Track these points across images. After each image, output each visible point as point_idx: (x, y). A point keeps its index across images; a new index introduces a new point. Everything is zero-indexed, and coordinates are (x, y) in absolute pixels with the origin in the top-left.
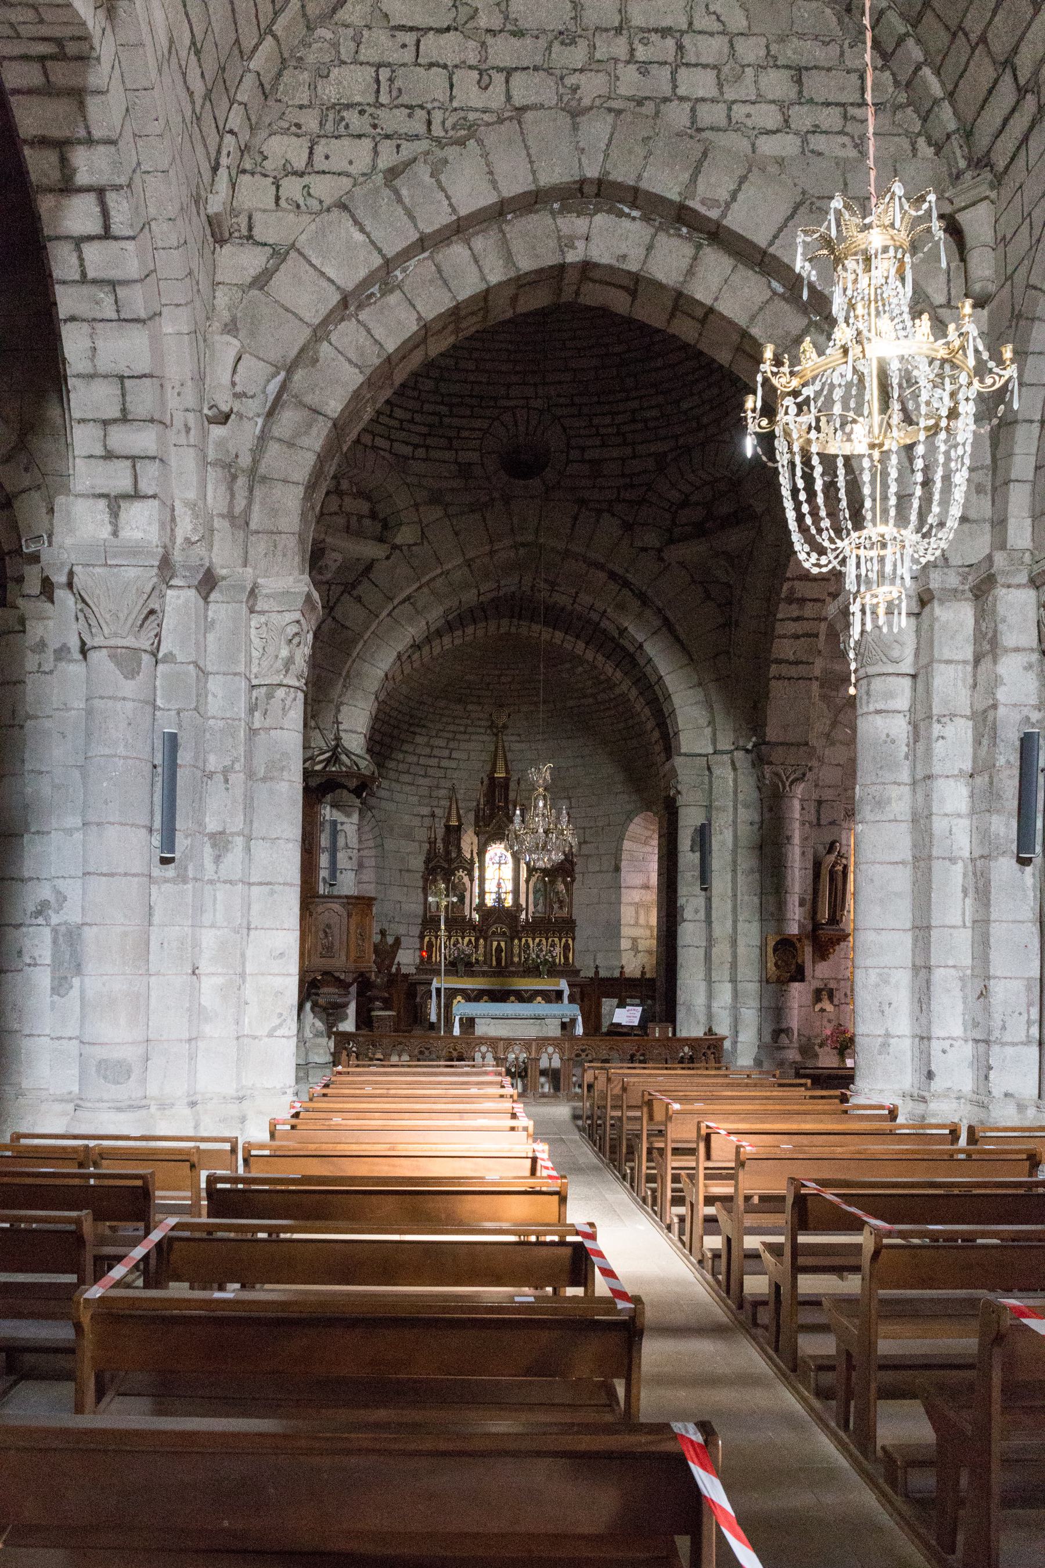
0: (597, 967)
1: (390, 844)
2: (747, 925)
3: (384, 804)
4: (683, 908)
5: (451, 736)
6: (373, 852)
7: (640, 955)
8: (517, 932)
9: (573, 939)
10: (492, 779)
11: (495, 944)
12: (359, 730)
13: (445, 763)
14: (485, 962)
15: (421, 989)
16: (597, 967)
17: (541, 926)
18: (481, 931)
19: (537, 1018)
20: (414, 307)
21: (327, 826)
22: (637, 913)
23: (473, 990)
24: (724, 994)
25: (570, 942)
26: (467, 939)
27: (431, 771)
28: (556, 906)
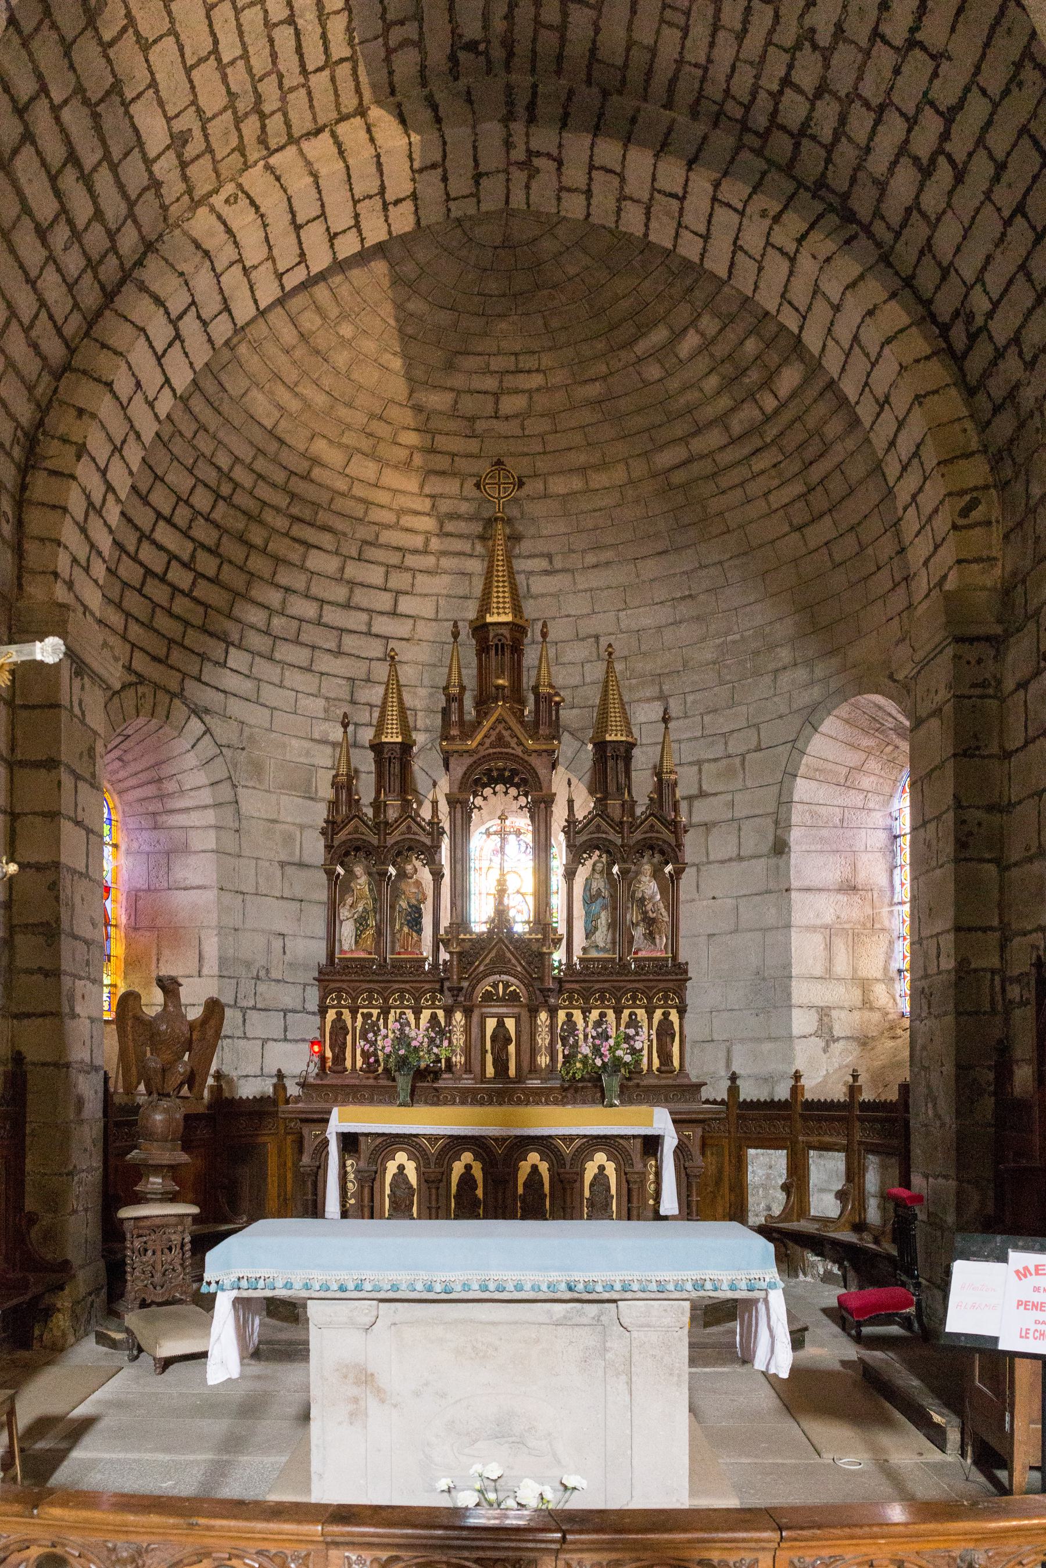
0: (734, 1078)
1: (253, 803)
3: (235, 707)
5: (394, 559)
6: (210, 817)
7: (837, 1047)
8: (545, 992)
9: (682, 1012)
10: (480, 629)
11: (491, 1024)
14: (468, 1068)
15: (310, 1132)
16: (734, 1078)
17: (605, 982)
18: (456, 991)
19: (581, 1297)
22: (829, 947)
23: (433, 1139)
25: (674, 1016)
27: (350, 642)
28: (639, 932)
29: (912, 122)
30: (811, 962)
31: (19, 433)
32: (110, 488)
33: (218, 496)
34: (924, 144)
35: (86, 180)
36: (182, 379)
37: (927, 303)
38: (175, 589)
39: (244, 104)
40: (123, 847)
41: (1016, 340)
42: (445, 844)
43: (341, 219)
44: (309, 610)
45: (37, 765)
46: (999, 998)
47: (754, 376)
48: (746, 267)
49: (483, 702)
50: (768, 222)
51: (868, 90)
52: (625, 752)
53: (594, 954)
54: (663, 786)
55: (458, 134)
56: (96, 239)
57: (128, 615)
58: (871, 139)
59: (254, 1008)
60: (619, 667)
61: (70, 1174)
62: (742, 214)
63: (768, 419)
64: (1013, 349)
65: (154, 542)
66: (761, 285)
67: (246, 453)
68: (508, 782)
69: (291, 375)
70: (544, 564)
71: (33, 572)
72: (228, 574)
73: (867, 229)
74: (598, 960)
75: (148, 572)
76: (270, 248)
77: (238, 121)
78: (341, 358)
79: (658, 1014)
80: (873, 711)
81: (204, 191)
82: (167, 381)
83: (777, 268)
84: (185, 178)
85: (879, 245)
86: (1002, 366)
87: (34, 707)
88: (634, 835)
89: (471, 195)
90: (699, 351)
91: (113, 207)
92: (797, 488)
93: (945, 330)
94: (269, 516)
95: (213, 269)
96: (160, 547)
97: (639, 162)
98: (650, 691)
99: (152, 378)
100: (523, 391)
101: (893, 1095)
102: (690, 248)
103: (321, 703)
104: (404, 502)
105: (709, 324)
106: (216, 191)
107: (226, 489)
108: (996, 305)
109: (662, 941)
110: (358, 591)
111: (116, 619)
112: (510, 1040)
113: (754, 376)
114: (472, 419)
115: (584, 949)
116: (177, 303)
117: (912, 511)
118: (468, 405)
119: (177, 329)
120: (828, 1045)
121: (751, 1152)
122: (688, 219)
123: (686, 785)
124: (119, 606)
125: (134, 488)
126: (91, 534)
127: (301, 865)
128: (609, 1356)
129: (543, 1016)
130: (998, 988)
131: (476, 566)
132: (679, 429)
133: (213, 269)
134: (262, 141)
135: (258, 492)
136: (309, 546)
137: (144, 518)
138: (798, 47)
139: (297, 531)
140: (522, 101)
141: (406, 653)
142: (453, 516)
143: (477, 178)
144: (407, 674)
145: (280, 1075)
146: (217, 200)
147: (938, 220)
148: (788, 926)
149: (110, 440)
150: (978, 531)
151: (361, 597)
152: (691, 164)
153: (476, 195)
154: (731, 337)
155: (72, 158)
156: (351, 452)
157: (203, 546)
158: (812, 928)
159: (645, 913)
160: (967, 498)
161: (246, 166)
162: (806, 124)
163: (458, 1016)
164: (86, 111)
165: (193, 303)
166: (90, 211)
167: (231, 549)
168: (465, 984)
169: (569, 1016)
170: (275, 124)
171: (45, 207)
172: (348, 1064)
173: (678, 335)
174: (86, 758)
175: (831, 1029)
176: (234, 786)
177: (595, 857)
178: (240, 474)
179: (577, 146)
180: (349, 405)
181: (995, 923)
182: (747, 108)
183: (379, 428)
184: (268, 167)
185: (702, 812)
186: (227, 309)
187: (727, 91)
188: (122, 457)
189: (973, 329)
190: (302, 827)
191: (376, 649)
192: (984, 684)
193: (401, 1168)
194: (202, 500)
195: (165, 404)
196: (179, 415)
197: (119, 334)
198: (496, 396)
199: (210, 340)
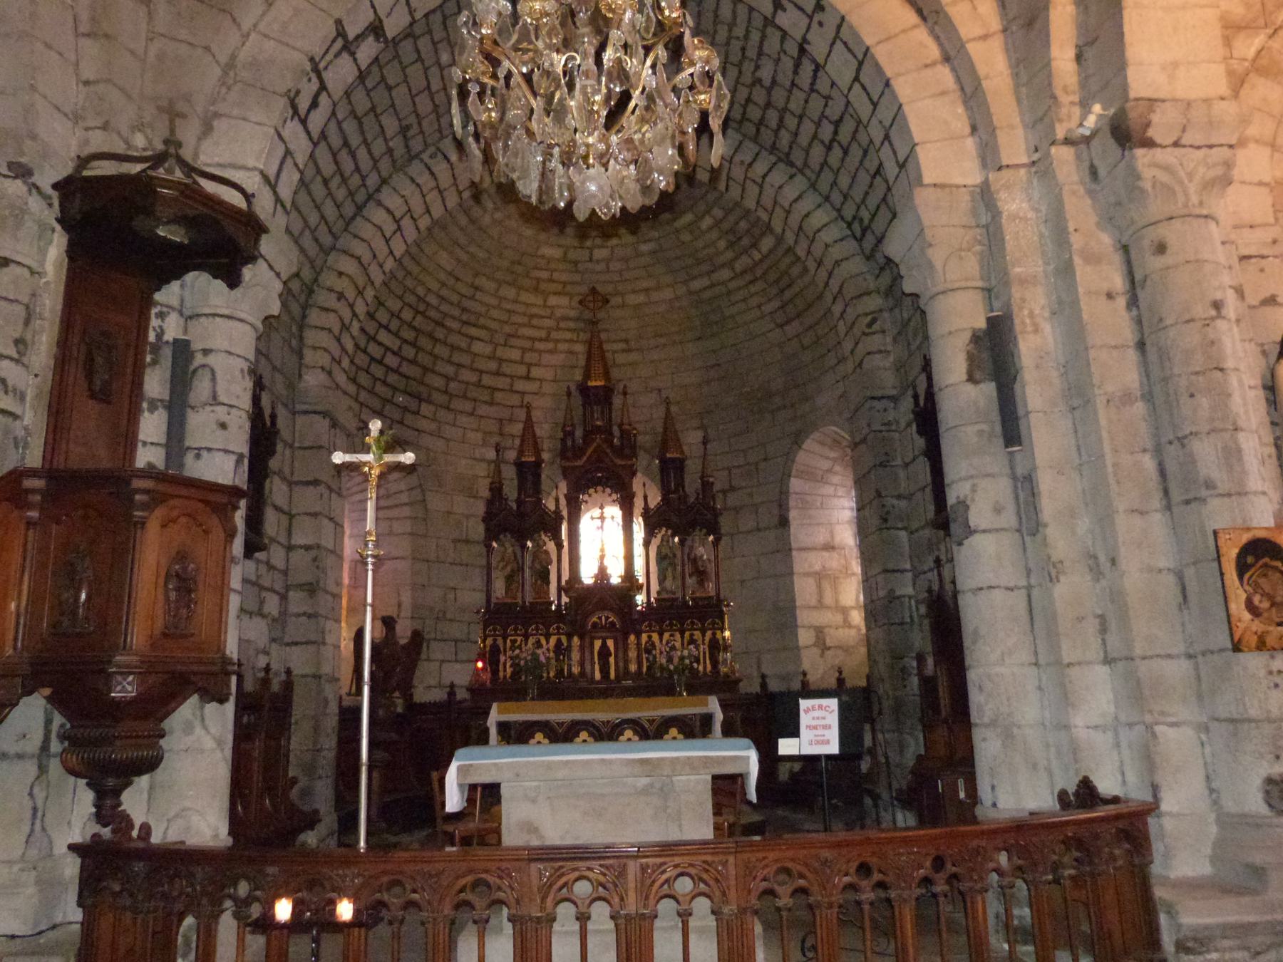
1: (436, 502)
2: (1137, 521)
4: (963, 505)
5: (528, 344)
11: (598, 644)
12: (251, 163)
13: (520, 385)
16: (763, 677)
17: (668, 613)
21: (167, 352)
22: (819, 587)
24: (1098, 695)
26: (553, 640)
32: (355, 315)
33: (417, 312)
36: (399, 248)
38: (389, 369)
42: (564, 527)
44: (473, 378)
45: (308, 483)
47: (746, 241)
49: (588, 436)
51: (792, 106)
53: (665, 596)
54: (706, 486)
56: (355, 180)
59: (435, 639)
60: (674, 409)
63: (756, 264)
67: (435, 286)
68: (605, 485)
69: (463, 241)
71: (307, 367)
73: (801, 171)
75: (373, 359)
76: (455, 179)
79: (709, 634)
82: (391, 252)
85: (809, 179)
87: (305, 448)
88: (681, 517)
92: (776, 304)
93: (849, 225)
94: (449, 323)
96: (380, 344)
98: (695, 423)
101: (863, 683)
103: (480, 435)
104: (535, 310)
106: (424, 151)
107: (422, 307)
108: (874, 216)
109: (711, 586)
110: (504, 365)
111: (352, 389)
113: (746, 241)
114: (576, 263)
117: (841, 322)
127: (467, 541)
128: (669, 811)
129: (632, 638)
131: (580, 348)
132: (705, 267)
135: (442, 308)
136: (472, 338)
138: (753, 84)
139: (465, 329)
141: (537, 402)
144: (537, 415)
145: (452, 686)
146: (425, 156)
148: (791, 574)
151: (506, 369)
154: (732, 218)
155: (346, 144)
158: (807, 574)
161: (442, 138)
163: (576, 640)
164: (355, 121)
166: (352, 167)
167: (424, 342)
169: (650, 637)
172: (501, 674)
173: (700, 218)
176: (423, 491)
177: (663, 532)
178: (433, 300)
181: (908, 566)
183: (519, 269)
185: (732, 500)
186: (428, 211)
190: (467, 517)
191: (516, 400)
192: (889, 424)
194: (407, 315)
195: (390, 264)
199: (417, 229)
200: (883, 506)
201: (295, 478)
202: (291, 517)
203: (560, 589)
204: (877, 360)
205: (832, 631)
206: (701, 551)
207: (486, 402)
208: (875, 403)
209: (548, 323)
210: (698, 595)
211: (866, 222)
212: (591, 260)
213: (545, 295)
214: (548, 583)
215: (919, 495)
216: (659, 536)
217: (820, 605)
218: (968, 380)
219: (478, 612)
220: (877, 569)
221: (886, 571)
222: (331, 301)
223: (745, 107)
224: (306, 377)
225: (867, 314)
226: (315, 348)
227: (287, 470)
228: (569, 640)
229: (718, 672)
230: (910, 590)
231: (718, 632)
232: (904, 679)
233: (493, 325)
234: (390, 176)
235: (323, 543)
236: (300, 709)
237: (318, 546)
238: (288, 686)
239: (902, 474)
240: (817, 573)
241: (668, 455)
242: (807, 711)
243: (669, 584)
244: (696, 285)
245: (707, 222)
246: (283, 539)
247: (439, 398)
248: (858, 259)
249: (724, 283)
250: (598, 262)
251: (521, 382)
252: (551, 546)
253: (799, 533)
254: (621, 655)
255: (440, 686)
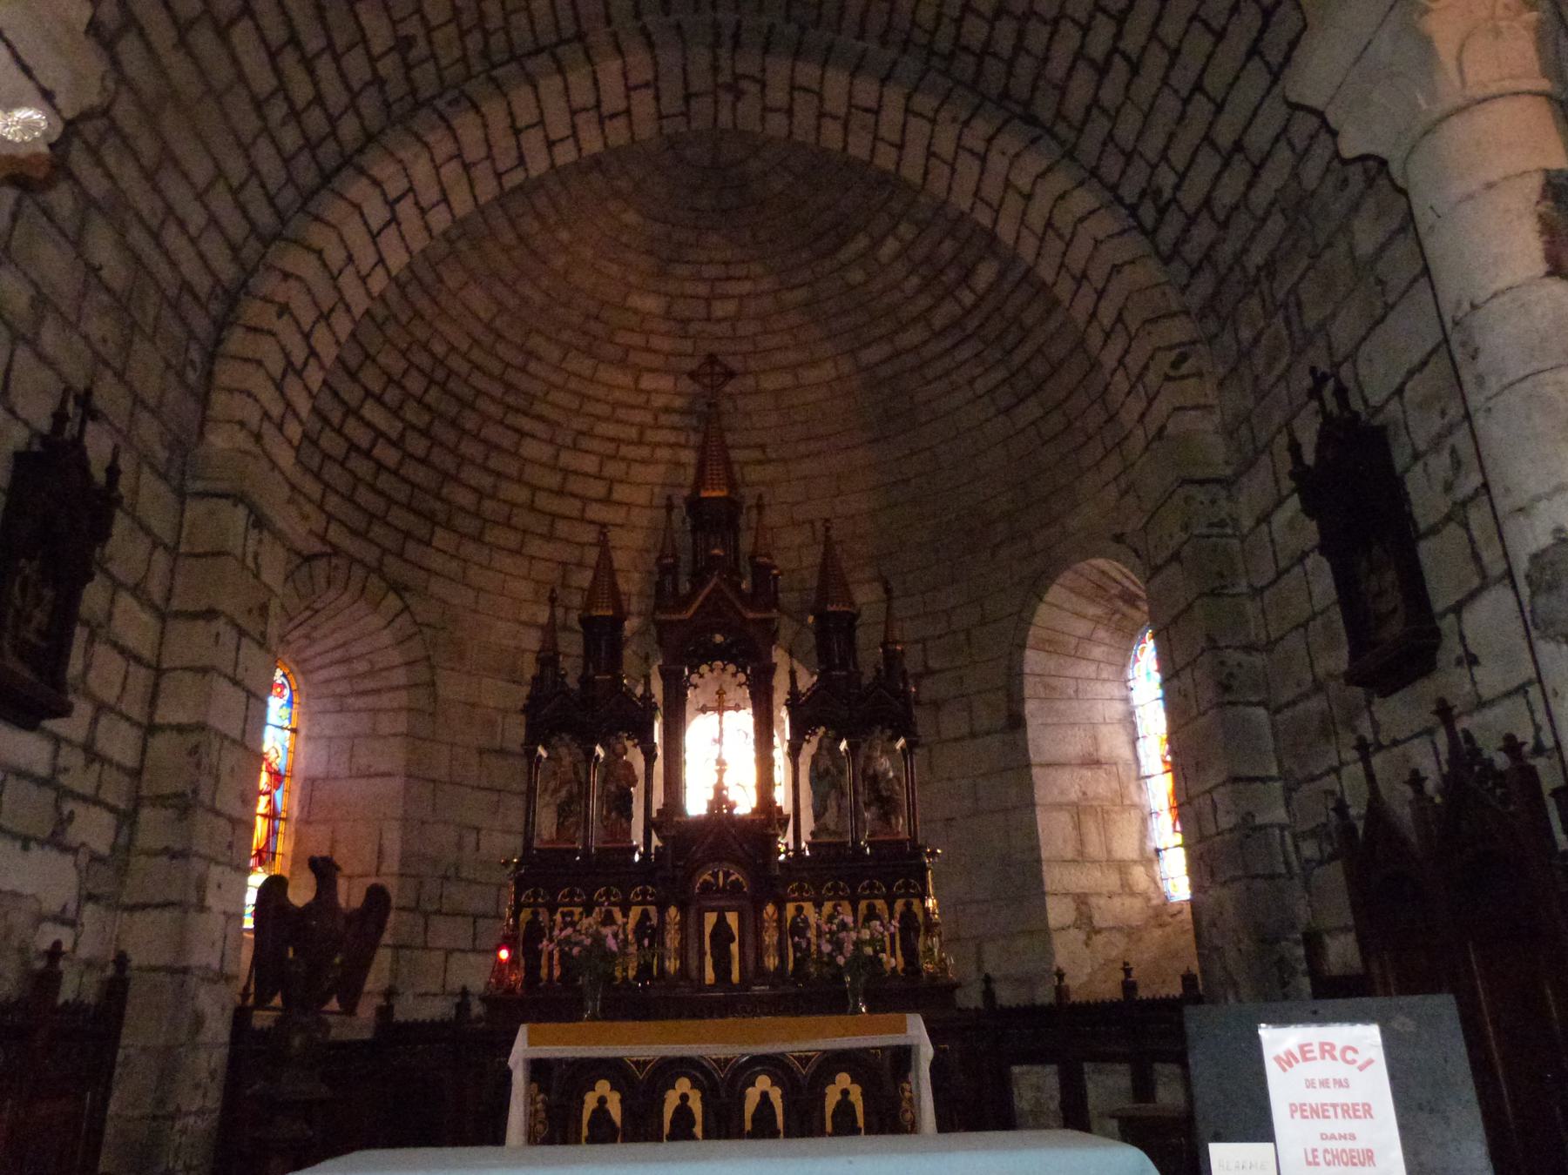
1: (452, 687)
3: (438, 587)
11: (711, 919)
17: (836, 868)
20: (173, 578)
22: (1078, 826)
26: (635, 912)
27: (562, 528)
29: (1086, 29)
30: (1060, 843)
31: (219, 291)
32: (313, 353)
34: (1099, 45)
35: (308, 64)
37: (1113, 188)
38: (380, 466)
39: (467, 19)
40: (303, 732)
41: (1207, 202)
43: (559, 128)
44: (522, 495)
45: (195, 616)
46: (1293, 857)
47: (951, 275)
48: (940, 171)
49: (698, 579)
50: (958, 126)
52: (849, 622)
53: (825, 839)
54: (892, 659)
55: (669, 57)
57: (327, 485)
58: (1048, 49)
59: (439, 912)
61: (172, 1117)
62: (933, 121)
63: (968, 312)
64: (1205, 214)
65: (361, 418)
66: (954, 186)
70: (757, 454)
71: (216, 421)
72: (437, 457)
74: (829, 845)
76: (490, 147)
77: (463, 34)
78: (559, 262)
79: (899, 905)
80: (1095, 577)
81: (428, 95)
83: (968, 167)
84: (408, 79)
85: (1062, 143)
86: (1195, 231)
87: (198, 556)
88: (843, 710)
89: (682, 114)
90: (897, 256)
91: (336, 97)
92: (999, 374)
93: (1133, 210)
94: (482, 403)
95: (433, 160)
97: (836, 83)
99: (366, 258)
100: (733, 297)
102: (886, 159)
105: (906, 230)
106: (440, 95)
107: (440, 375)
108: (1182, 177)
111: (312, 488)
112: (733, 940)
113: (951, 275)
115: (812, 834)
116: (394, 188)
117: (1119, 376)
118: (682, 309)
119: (393, 211)
120: (1089, 938)
121: (1016, 1069)
122: (884, 131)
123: (912, 664)
124: (317, 476)
125: (338, 358)
126: (287, 391)
129: (770, 909)
130: (1291, 848)
131: (688, 456)
133: (433, 160)
134: (485, 54)
136: (522, 434)
137: (351, 393)
139: (511, 419)
140: (727, 33)
141: (616, 537)
142: (667, 410)
143: (687, 98)
144: (620, 559)
145: (465, 992)
147: (1118, 111)
149: (316, 304)
150: (1193, 381)
151: (575, 485)
152: (884, 81)
153: (685, 114)
155: (294, 40)
156: (567, 348)
157: (413, 427)
158: (1059, 806)
159: (878, 791)
160: (1177, 351)
161: (469, 77)
162: (988, 42)
163: (673, 911)
165: (411, 189)
167: (440, 430)
168: (679, 873)
169: (799, 909)
170: (498, 41)
171: (264, 81)
172: (544, 972)
173: (877, 243)
174: (256, 613)
175: (1090, 918)
178: (455, 362)
179: (779, 70)
180: (567, 305)
181: (1274, 771)
182: (933, 33)
184: (492, 79)
185: (930, 689)
187: (914, 23)
188: (329, 325)
189: (1162, 202)
192: (1222, 524)
193: (602, 1101)
194: (415, 384)
195: (378, 282)
196: (393, 296)
197: (335, 210)
198: (708, 301)
200: (1222, 663)
201: (175, 604)
202: (159, 671)
203: (649, 825)
204: (1189, 419)
205: (1102, 902)
206: (884, 763)
207: (542, 536)
208: (1193, 490)
209: (639, 416)
210: (881, 838)
211: (1167, 194)
212: (708, 319)
213: (639, 372)
214: (629, 817)
215: (1295, 641)
216: (815, 740)
217: (1081, 858)
218: (1549, 274)
219: (507, 864)
220: (1212, 777)
221: (1236, 780)
222: (269, 318)
223: (959, 22)
224: (211, 438)
225: (1171, 348)
226: (231, 391)
227: (156, 590)
228: (662, 911)
229: (918, 971)
230: (1280, 814)
231: (916, 902)
232: (1285, 984)
233: (554, 415)
234: (382, 131)
235: (214, 721)
236: (139, 1035)
237: (201, 727)
238: (116, 988)
239: (1251, 608)
240: (1075, 805)
241: (830, 608)
242: (1287, 1061)
243: (830, 818)
244: (870, 355)
245: (890, 247)
246: (136, 712)
247: (468, 525)
248: (1153, 264)
249: (915, 348)
250: (719, 321)
251: (595, 506)
252: (636, 758)
253: (1042, 739)
254: (750, 939)
255: (444, 993)
